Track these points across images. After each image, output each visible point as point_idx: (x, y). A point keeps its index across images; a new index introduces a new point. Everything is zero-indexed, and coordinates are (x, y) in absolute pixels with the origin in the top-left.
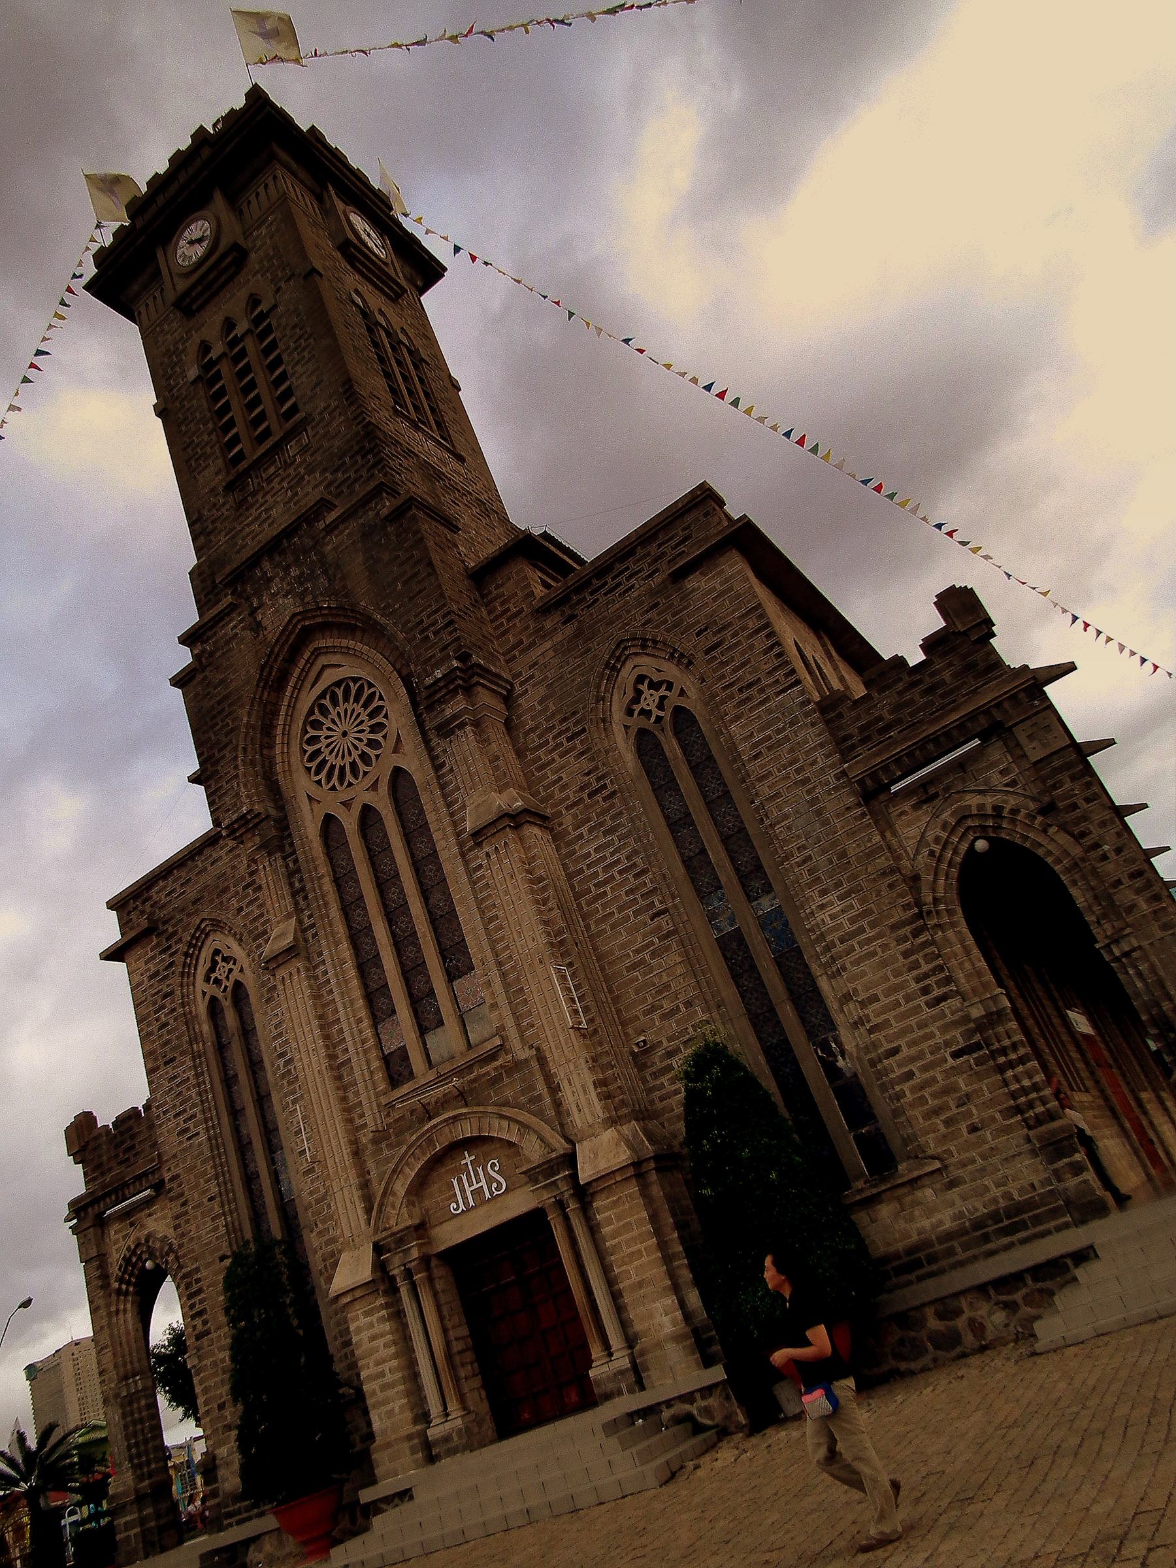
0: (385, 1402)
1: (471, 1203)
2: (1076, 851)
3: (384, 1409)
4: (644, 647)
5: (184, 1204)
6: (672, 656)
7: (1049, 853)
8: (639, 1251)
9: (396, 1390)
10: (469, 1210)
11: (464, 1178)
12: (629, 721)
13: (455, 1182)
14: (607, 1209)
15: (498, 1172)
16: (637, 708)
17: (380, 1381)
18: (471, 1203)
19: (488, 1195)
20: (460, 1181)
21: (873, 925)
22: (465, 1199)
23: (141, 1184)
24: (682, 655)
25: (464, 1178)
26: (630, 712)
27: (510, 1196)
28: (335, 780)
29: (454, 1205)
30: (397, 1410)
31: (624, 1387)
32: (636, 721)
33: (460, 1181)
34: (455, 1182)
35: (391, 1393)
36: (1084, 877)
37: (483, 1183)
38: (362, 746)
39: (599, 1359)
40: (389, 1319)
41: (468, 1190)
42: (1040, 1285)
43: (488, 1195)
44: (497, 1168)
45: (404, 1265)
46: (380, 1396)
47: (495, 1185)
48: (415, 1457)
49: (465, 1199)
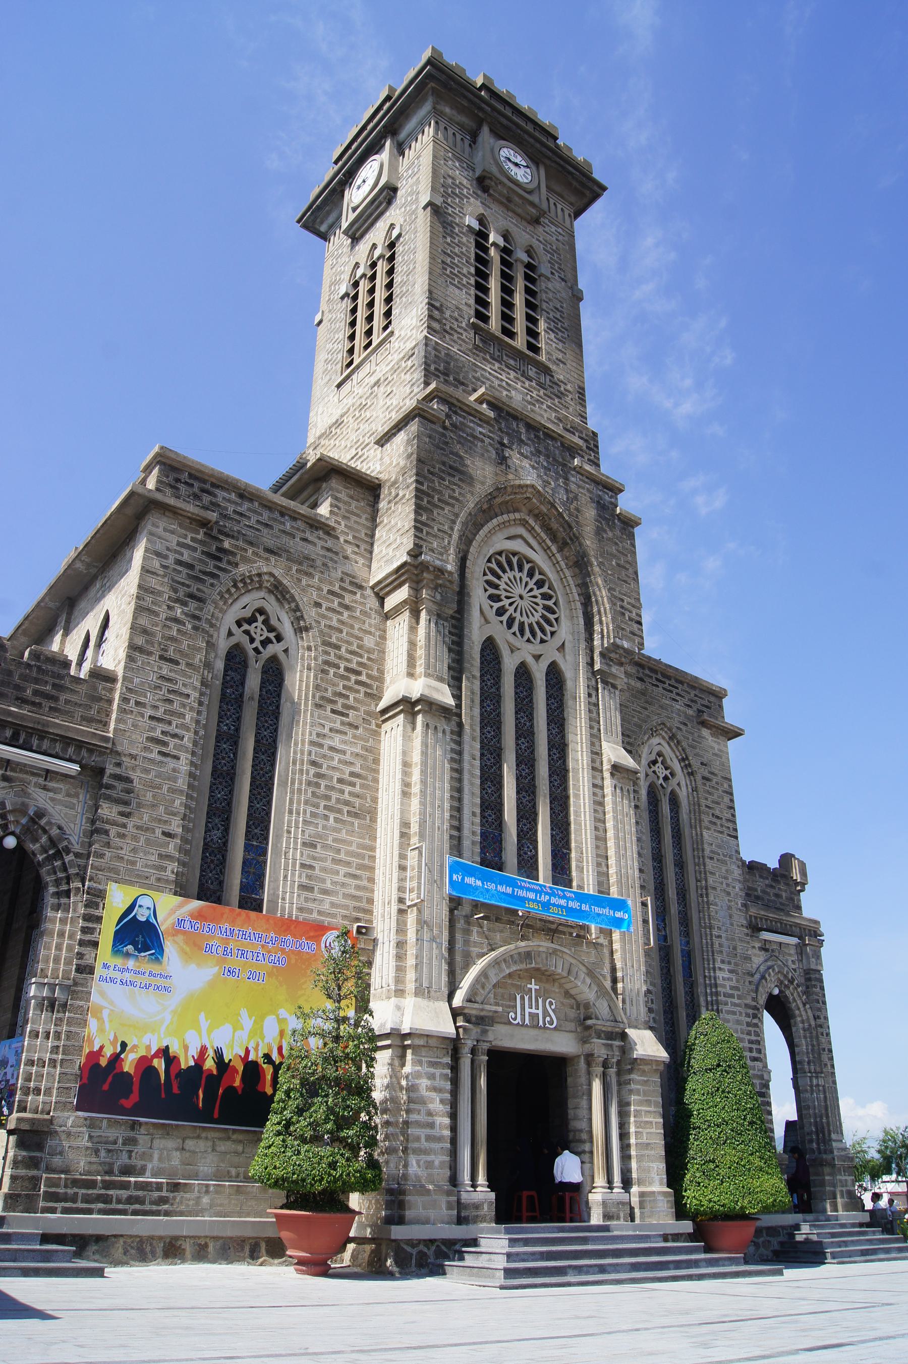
0: (426, 1152)
1: (527, 1022)
2: (813, 1023)
3: (424, 1158)
4: (670, 738)
5: (127, 815)
6: (683, 760)
7: (801, 1016)
8: (651, 1122)
9: (441, 1145)
10: (523, 1025)
11: (526, 998)
12: (235, 629)
13: (518, 997)
14: (638, 1082)
15: (553, 1010)
16: (246, 627)
17: (428, 1131)
18: (527, 1022)
19: (541, 1023)
20: (522, 998)
21: (739, 997)
22: (523, 1015)
23: (65, 750)
24: (690, 765)
25: (526, 998)
26: (239, 624)
27: (556, 1034)
28: (548, 628)
29: (512, 1014)
30: (437, 1163)
31: (622, 1215)
32: (239, 636)
33: (522, 998)
34: (518, 997)
35: (436, 1146)
36: (811, 1037)
37: (540, 1012)
38: (506, 602)
39: (482, 1186)
40: (116, 1059)
41: (527, 1010)
42: (768, 1238)
43: (541, 1023)
44: (553, 1007)
45: (478, 1041)
46: (424, 1144)
47: (548, 1019)
48: (450, 1212)
49: (523, 1015)
